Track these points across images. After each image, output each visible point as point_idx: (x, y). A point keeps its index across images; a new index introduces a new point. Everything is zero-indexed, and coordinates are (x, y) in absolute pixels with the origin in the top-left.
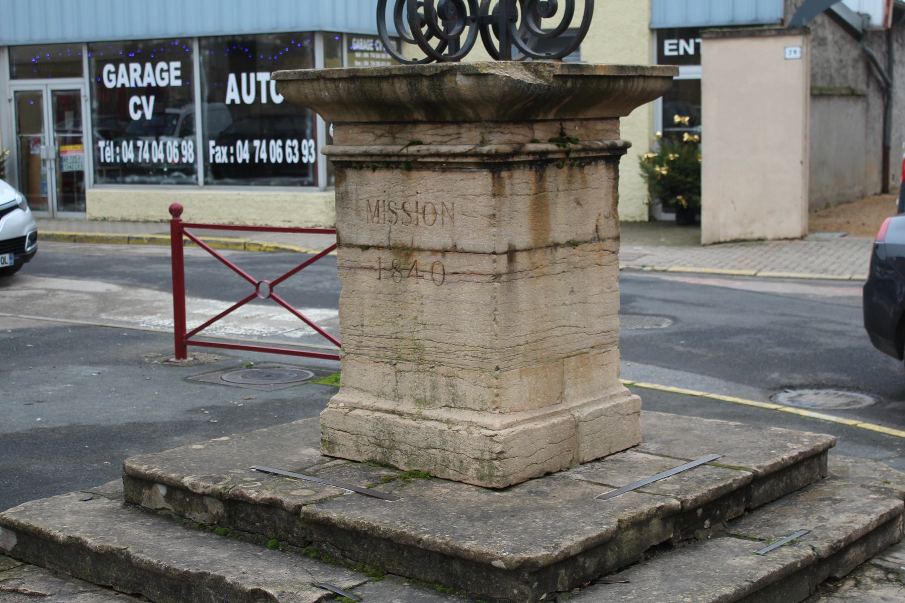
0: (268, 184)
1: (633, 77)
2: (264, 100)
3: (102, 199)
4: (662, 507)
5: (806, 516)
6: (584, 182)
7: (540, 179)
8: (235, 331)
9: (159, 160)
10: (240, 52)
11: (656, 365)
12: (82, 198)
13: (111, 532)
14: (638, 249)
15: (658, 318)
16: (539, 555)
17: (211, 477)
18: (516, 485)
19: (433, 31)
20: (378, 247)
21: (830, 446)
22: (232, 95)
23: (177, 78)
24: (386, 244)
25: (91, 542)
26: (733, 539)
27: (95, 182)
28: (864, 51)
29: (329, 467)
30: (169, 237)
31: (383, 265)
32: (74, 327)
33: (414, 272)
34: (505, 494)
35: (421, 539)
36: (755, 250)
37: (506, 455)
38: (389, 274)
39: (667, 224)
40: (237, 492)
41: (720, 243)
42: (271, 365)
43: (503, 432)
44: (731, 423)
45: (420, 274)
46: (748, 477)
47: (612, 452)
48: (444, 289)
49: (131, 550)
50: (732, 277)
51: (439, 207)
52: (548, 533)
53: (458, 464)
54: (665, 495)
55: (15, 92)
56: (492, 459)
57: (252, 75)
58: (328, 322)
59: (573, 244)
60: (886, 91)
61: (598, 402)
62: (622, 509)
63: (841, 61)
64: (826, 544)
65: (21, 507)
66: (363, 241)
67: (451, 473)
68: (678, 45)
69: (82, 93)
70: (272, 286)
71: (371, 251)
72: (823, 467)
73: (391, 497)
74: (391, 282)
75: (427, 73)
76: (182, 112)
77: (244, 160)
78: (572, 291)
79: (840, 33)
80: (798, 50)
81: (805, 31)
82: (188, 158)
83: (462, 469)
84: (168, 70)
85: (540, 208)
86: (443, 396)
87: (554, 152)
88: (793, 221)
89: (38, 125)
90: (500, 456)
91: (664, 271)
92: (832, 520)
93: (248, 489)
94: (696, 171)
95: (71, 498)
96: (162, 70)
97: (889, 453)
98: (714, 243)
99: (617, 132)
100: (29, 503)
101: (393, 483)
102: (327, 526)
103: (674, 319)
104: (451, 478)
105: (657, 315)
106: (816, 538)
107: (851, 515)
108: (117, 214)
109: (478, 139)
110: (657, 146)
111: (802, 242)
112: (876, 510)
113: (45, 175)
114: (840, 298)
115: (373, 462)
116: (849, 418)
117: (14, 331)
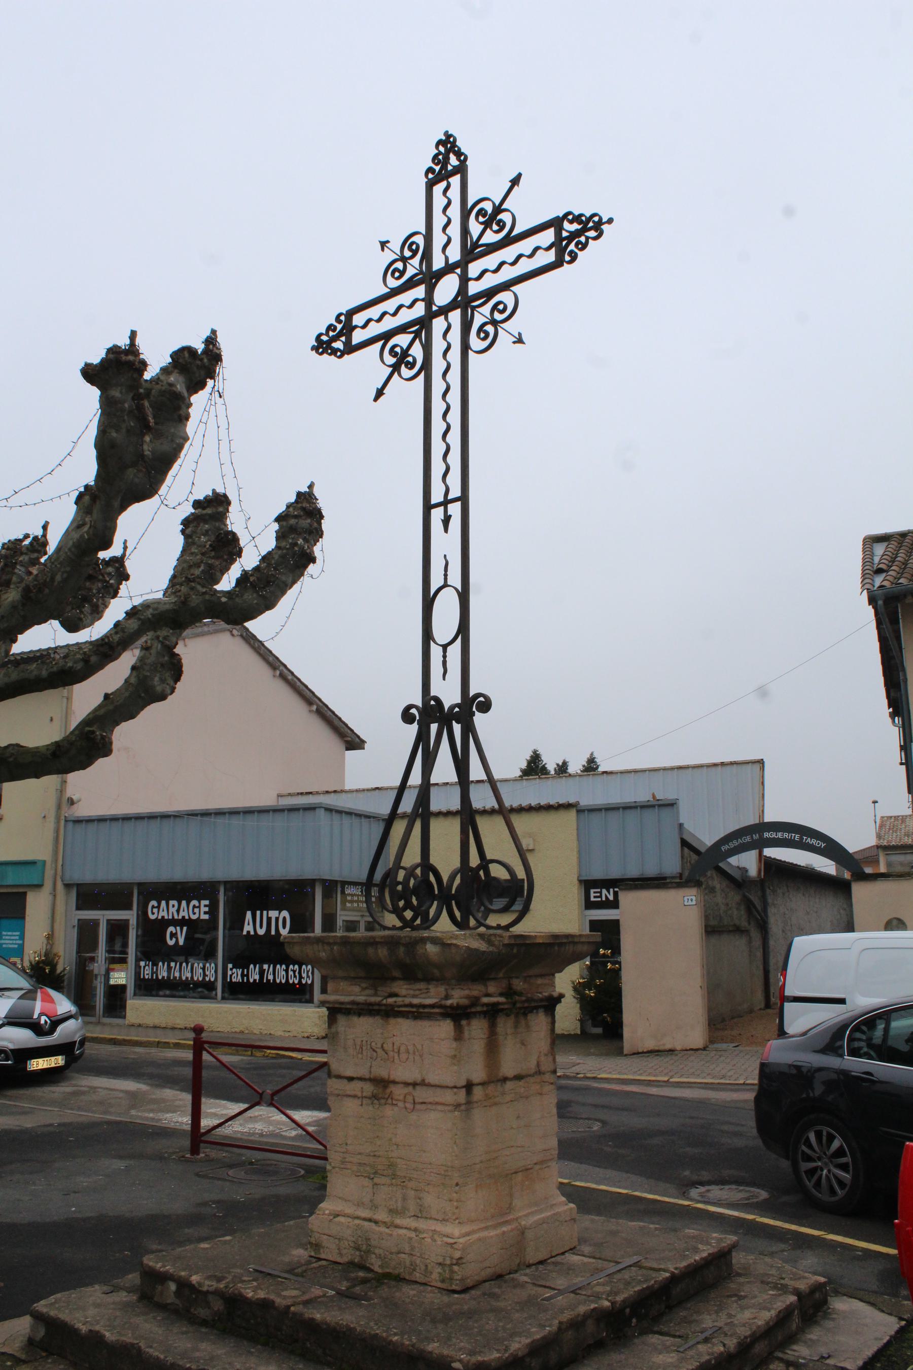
0: (273, 1000)
1: (565, 943)
2: (273, 933)
3: (140, 1009)
4: (595, 1309)
5: (717, 1312)
6: (528, 1027)
7: (492, 1026)
8: (240, 1129)
9: (187, 978)
10: (256, 894)
11: (589, 1164)
12: (124, 1007)
13: (127, 1326)
14: (573, 1058)
15: (590, 1122)
16: (492, 1357)
17: (215, 1276)
18: (473, 1287)
19: (409, 905)
20: (361, 1079)
21: (734, 1246)
22: (248, 928)
23: (205, 913)
24: (367, 1077)
25: (109, 1336)
26: (657, 1336)
27: (135, 995)
28: (744, 896)
29: (315, 1268)
30: (192, 1043)
31: (364, 1094)
32: (109, 1123)
33: (390, 1101)
34: (463, 1296)
35: (391, 1341)
36: (667, 1059)
37: (464, 1261)
38: (369, 1101)
39: (596, 1037)
40: (236, 1292)
41: (638, 1053)
42: (268, 1162)
43: (461, 1240)
44: (652, 1226)
45: (394, 1102)
46: (667, 1278)
47: (553, 1254)
48: (413, 1117)
49: (142, 1345)
50: (649, 1083)
51: (411, 1048)
52: (500, 1334)
53: (423, 1268)
54: (597, 1297)
55: (79, 920)
56: (452, 1264)
57: (265, 913)
58: (317, 1123)
59: (519, 1078)
60: (763, 927)
61: (540, 1211)
62: (562, 1311)
63: (727, 905)
64: (735, 1341)
65: (52, 1299)
66: (349, 1073)
67: (417, 1276)
68: (601, 892)
69: (131, 922)
70: (273, 1095)
71: (355, 1082)
72: (729, 1265)
73: (368, 1299)
74: (371, 1108)
75: (403, 941)
76: (208, 937)
77: (255, 980)
78: (518, 1117)
79: (725, 883)
80: (694, 898)
81: (698, 884)
82: (210, 977)
83: (427, 1272)
84: (199, 907)
85: (492, 1048)
86: (412, 1208)
87: (502, 1004)
88: (696, 1036)
89: (94, 946)
90: (459, 1262)
91: (594, 1078)
92: (739, 1316)
93: (245, 1289)
94: (617, 994)
95: (95, 1291)
96: (194, 907)
97: (782, 1246)
98: (634, 1054)
99: (553, 985)
100: (59, 1295)
101: (368, 1285)
102: (312, 1326)
103: (604, 1123)
104: (418, 1280)
105: (589, 1119)
106: (726, 1335)
107: (754, 1311)
108: (150, 1021)
109: (443, 994)
110: (586, 973)
111: (704, 1052)
112: (775, 1306)
113: (96, 988)
114: (736, 1101)
115: (351, 1263)
116: (748, 1213)
117: (60, 1125)
